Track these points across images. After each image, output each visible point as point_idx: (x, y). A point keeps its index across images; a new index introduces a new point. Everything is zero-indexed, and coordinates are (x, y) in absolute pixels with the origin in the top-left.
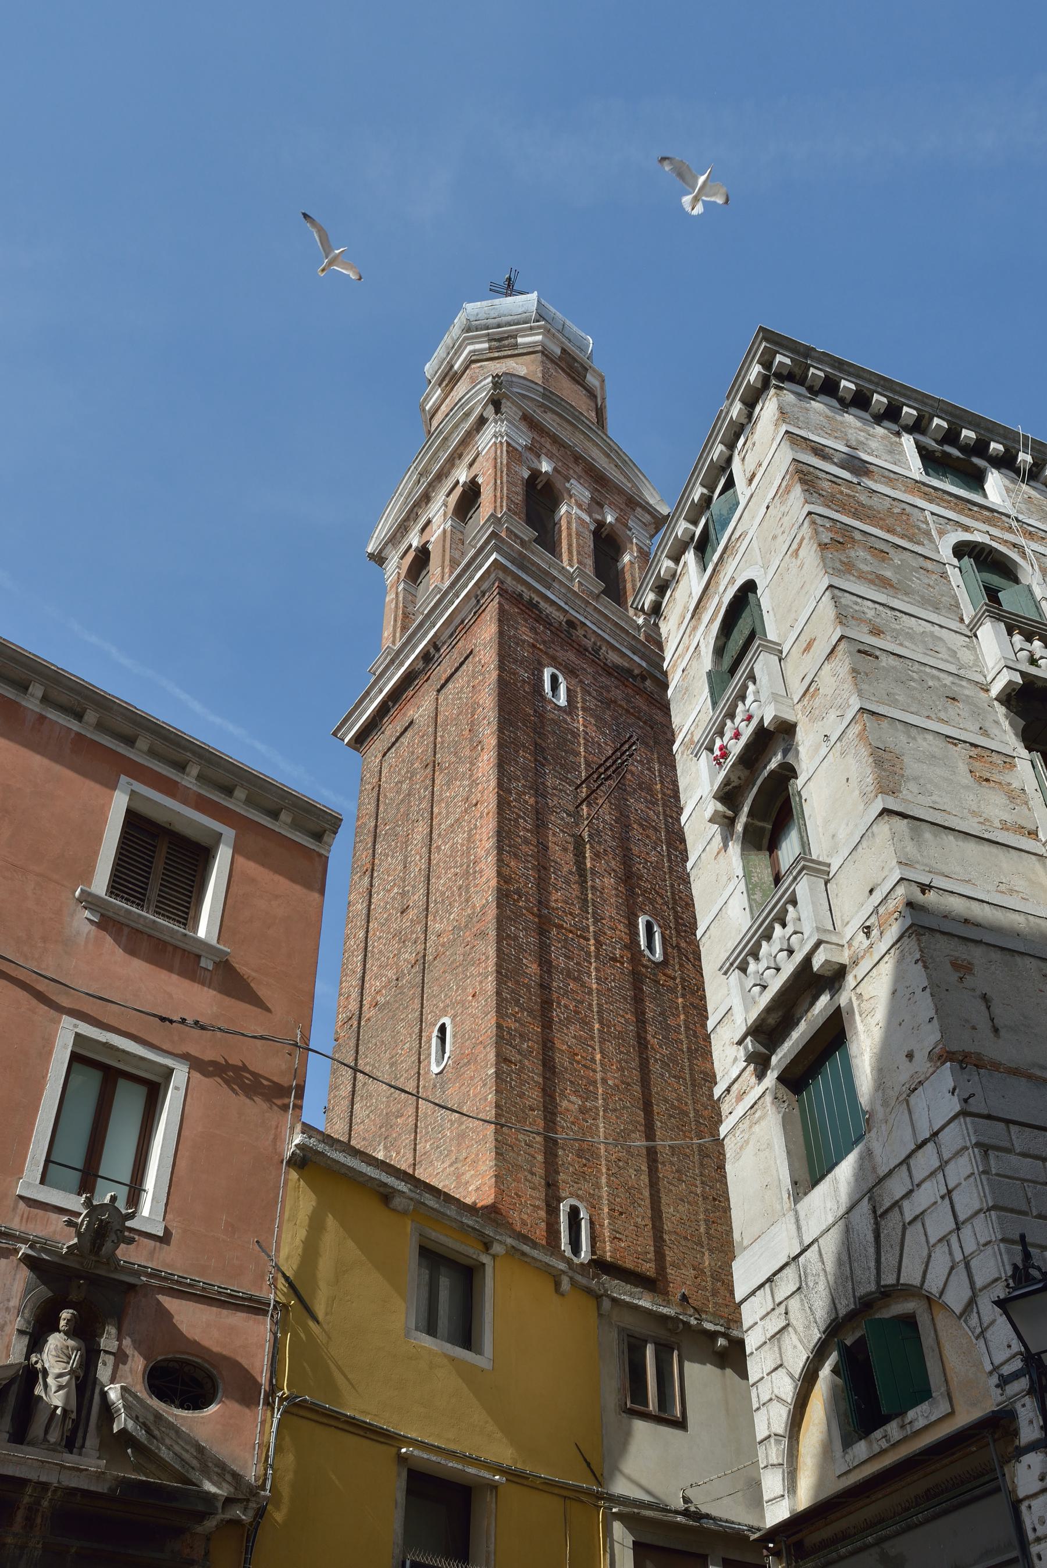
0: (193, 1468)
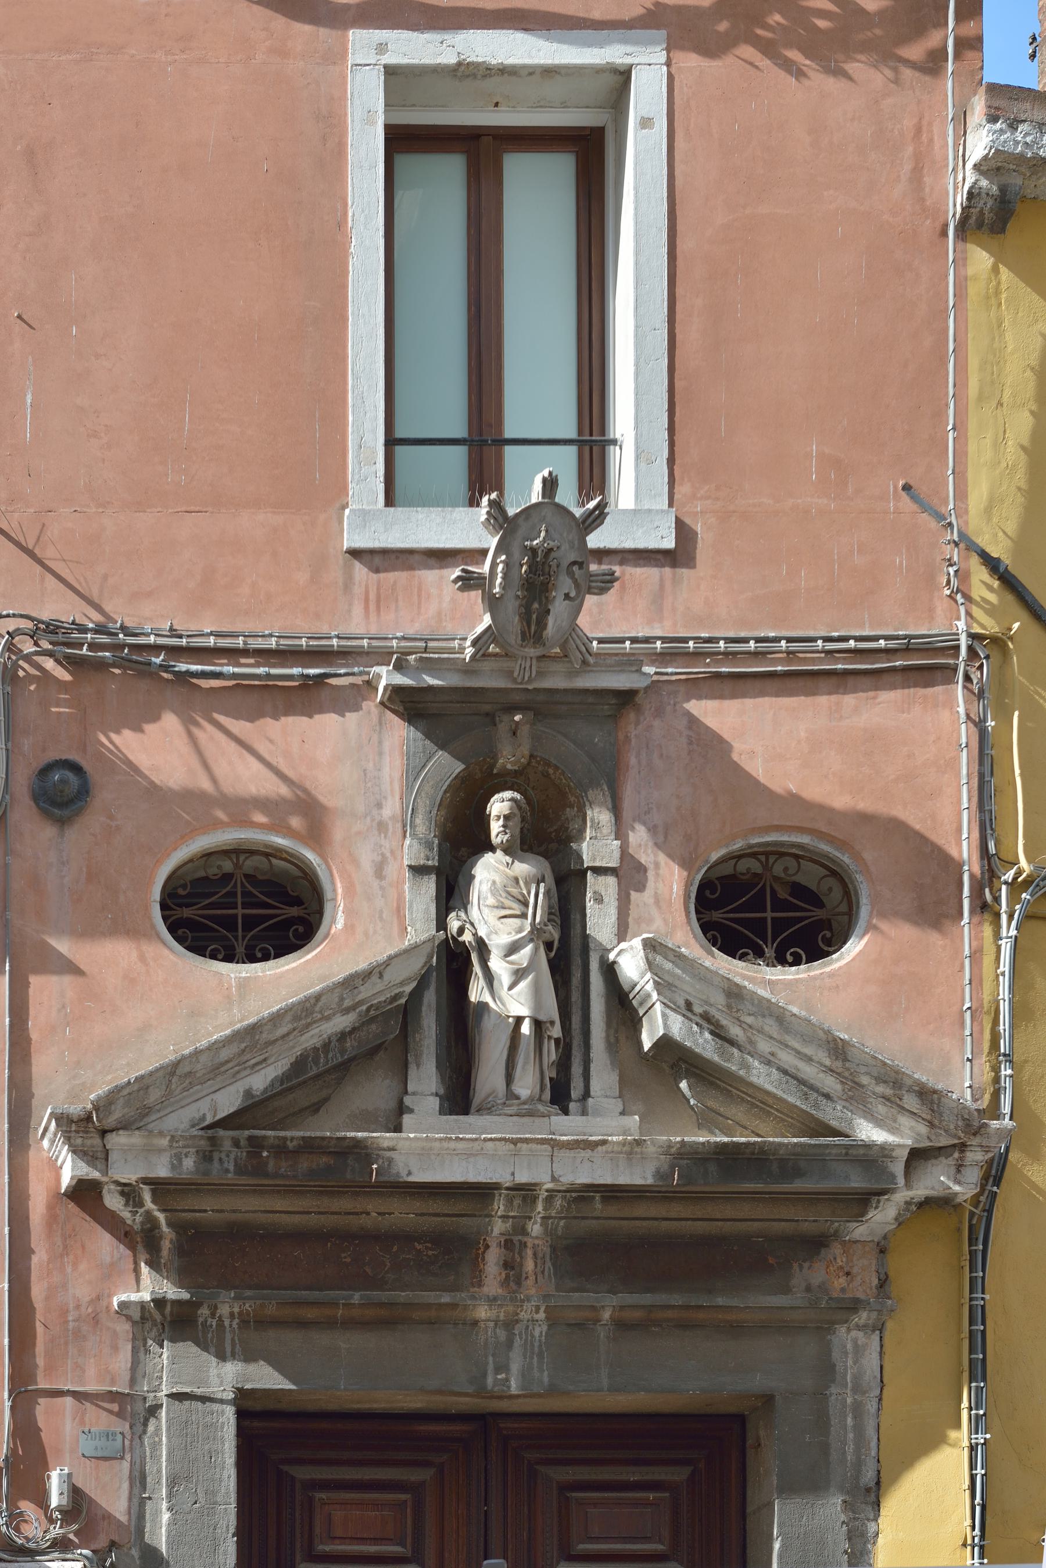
0: (827, 1096)
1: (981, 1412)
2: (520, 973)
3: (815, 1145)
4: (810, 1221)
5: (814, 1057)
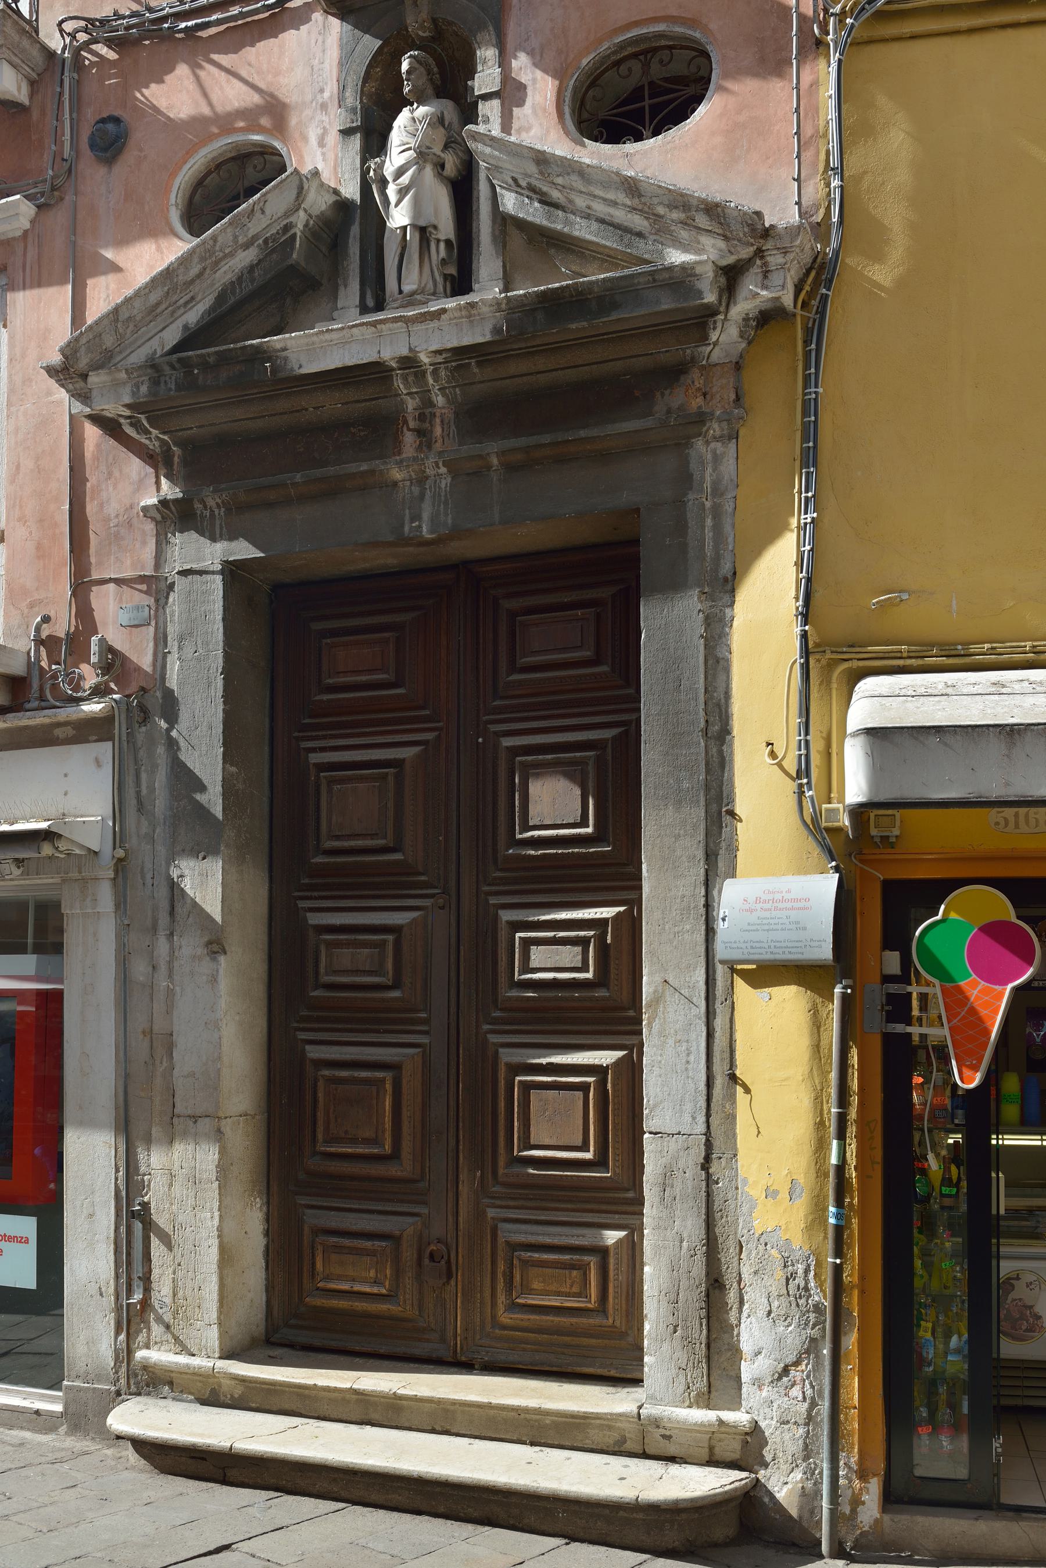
0: (640, 235)
1: (810, 494)
2: (404, 191)
3: (621, 277)
4: (662, 352)
5: (618, 201)
